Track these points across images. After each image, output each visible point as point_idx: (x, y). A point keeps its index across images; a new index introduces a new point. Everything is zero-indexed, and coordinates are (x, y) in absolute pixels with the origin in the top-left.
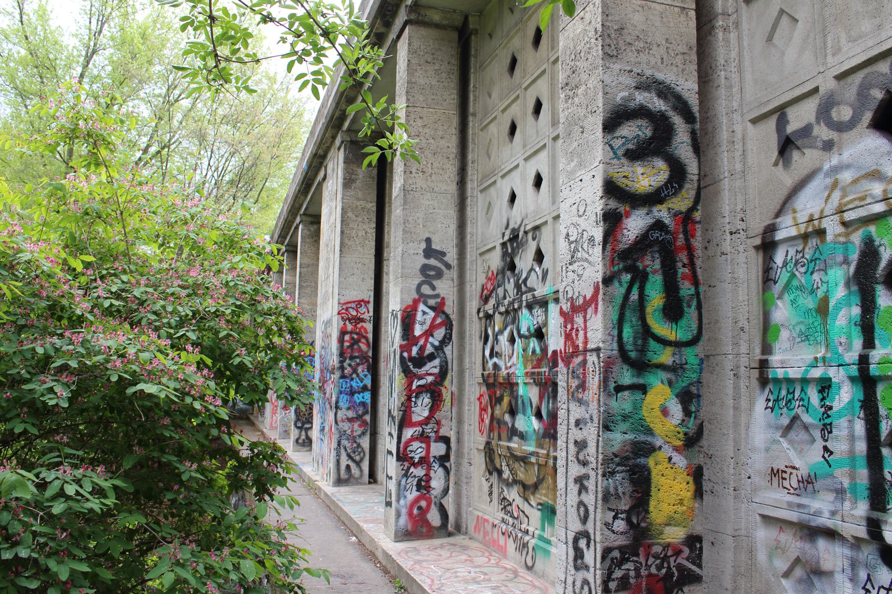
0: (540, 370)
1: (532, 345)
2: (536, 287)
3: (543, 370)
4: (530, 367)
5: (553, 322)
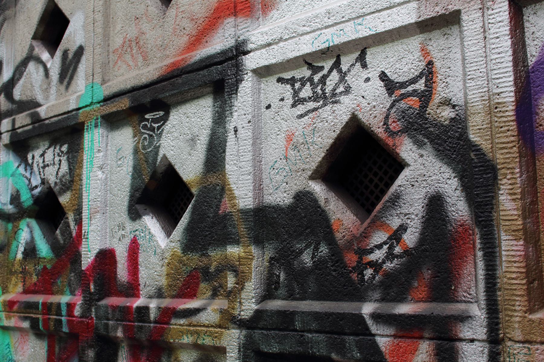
0: (53, 299)
1: (24, 236)
2: (40, 98)
3: (65, 299)
4: (20, 288)
5: (100, 174)
